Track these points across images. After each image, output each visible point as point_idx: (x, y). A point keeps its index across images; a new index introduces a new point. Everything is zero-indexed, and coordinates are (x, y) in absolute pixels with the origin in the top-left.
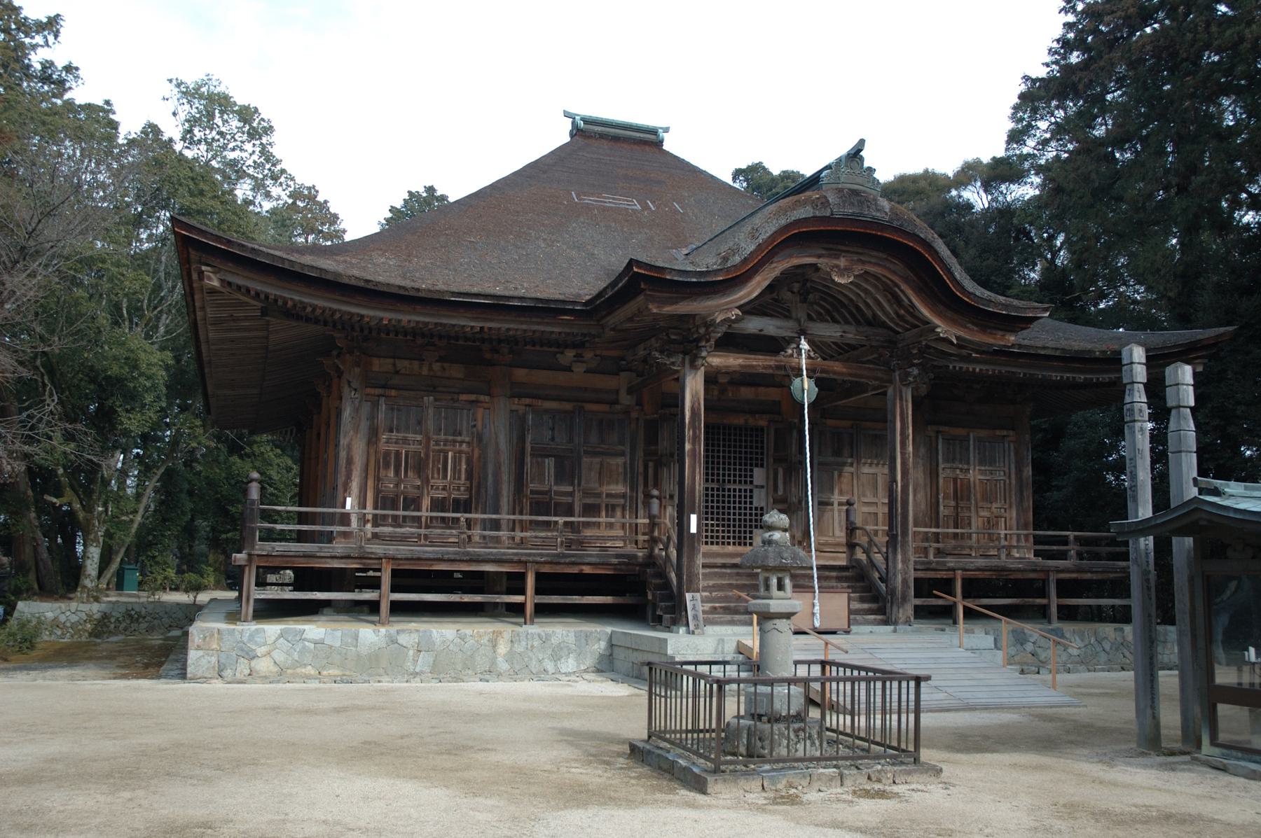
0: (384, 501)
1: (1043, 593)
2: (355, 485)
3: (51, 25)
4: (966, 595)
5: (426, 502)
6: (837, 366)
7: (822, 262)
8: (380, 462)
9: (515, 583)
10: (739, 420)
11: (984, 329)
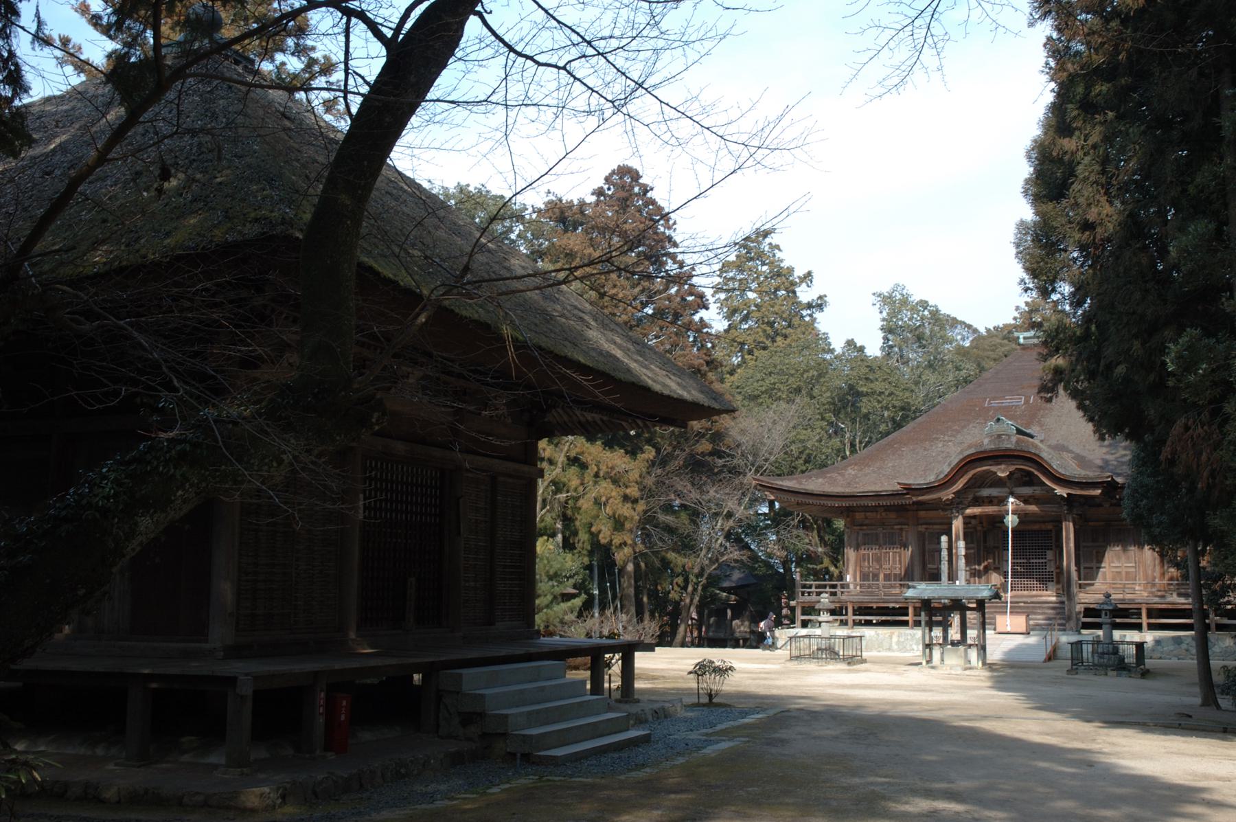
0: (864, 577)
1: (1139, 615)
2: (851, 570)
3: (808, 277)
4: (1149, 617)
5: (881, 576)
6: (1033, 508)
7: (994, 469)
8: (860, 561)
9: (904, 611)
10: (1036, 527)
11: (1082, 489)
